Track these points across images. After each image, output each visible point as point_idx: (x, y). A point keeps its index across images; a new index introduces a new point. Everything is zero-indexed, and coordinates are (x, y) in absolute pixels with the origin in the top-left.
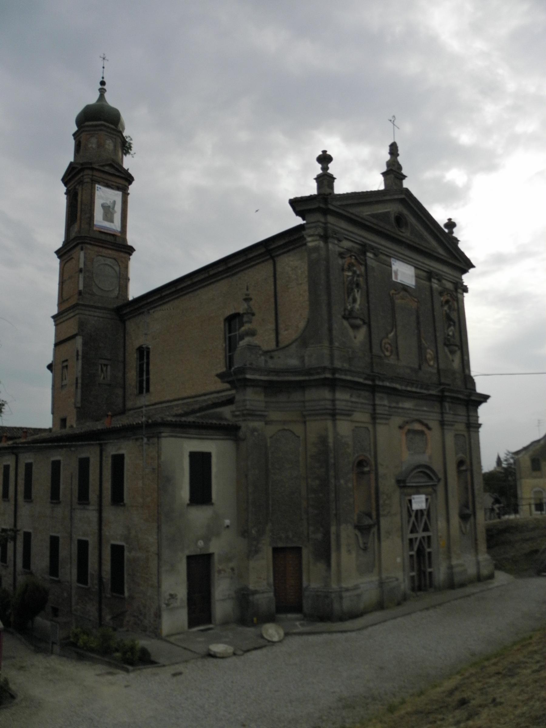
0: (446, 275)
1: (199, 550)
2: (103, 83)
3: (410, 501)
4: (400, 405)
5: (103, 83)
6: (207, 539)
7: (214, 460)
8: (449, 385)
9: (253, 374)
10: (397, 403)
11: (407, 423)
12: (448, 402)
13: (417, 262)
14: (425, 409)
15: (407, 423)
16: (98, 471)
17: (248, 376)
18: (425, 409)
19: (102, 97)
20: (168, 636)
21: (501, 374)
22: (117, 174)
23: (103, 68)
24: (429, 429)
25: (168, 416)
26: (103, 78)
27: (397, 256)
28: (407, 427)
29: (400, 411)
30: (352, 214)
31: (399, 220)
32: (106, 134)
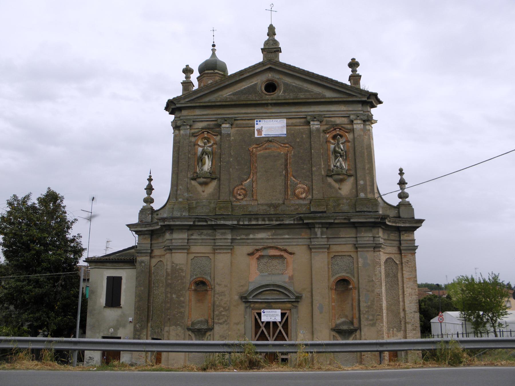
1: (110, 334)
2: (214, 46)
3: (259, 315)
4: (251, 236)
5: (214, 46)
6: (116, 328)
7: (124, 281)
8: (325, 212)
9: (136, 228)
10: (249, 235)
11: (257, 250)
12: (319, 227)
13: (287, 114)
14: (287, 236)
15: (257, 250)
18: (287, 236)
19: (214, 54)
21: (391, 193)
23: (214, 36)
26: (214, 42)
27: (260, 117)
30: (205, 102)
31: (271, 87)
32: (208, 78)
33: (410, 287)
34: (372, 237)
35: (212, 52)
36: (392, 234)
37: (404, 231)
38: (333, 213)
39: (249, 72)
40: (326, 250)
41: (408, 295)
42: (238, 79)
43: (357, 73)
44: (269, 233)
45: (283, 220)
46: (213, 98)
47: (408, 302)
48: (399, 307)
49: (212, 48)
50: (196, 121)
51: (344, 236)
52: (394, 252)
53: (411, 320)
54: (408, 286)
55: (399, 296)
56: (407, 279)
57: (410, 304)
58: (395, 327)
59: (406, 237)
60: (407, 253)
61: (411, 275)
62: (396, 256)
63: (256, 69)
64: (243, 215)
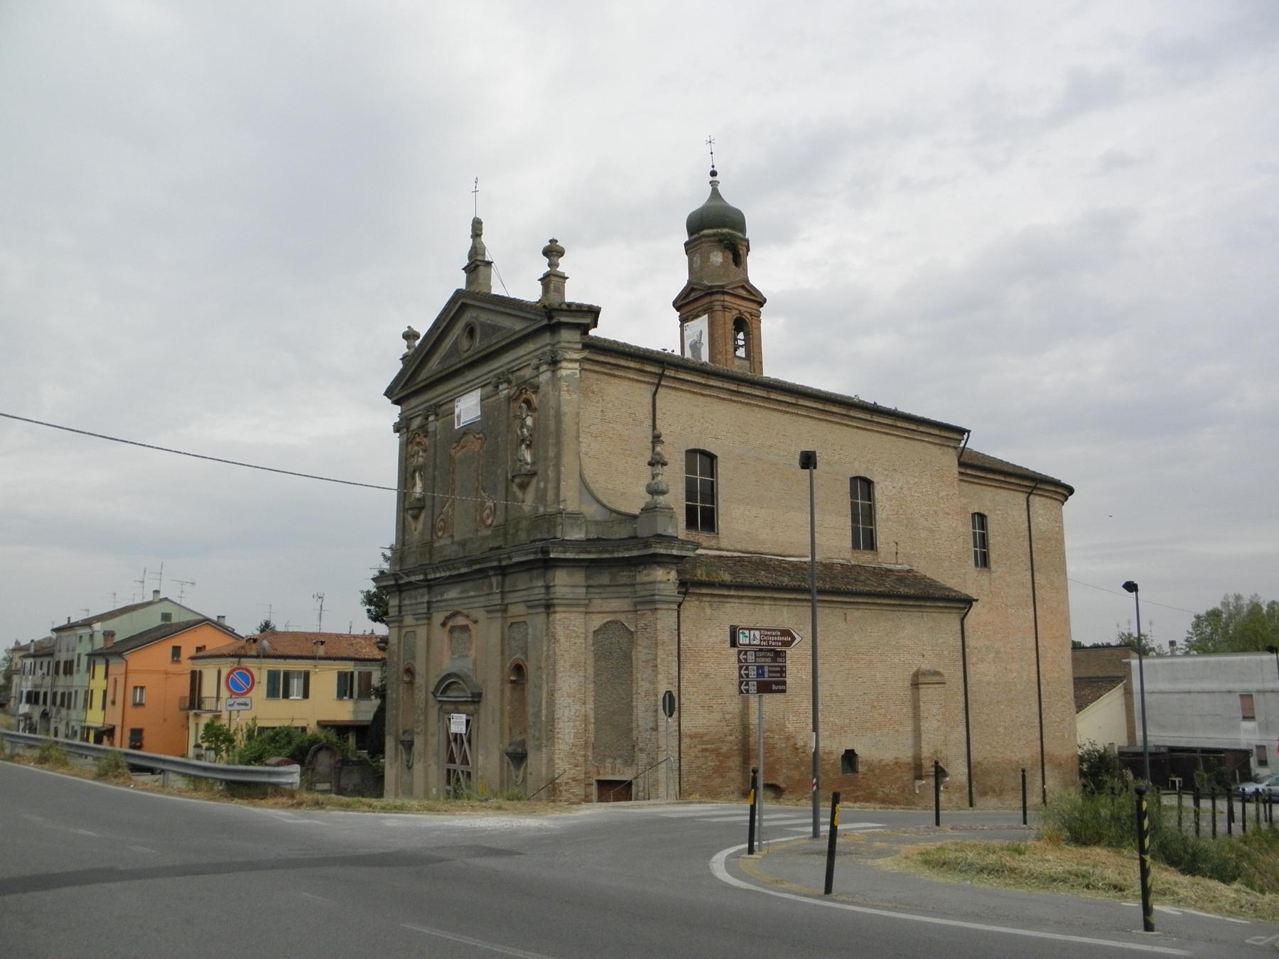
0: (513, 364)
2: (713, 174)
4: (445, 597)
5: (713, 174)
10: (442, 595)
14: (472, 593)
16: (122, 692)
17: (551, 556)
20: (215, 782)
22: (752, 298)
23: (712, 153)
24: (476, 622)
25: (746, 566)
26: (713, 167)
28: (450, 624)
29: (442, 604)
33: (646, 678)
34: (542, 586)
35: (710, 188)
36: (622, 574)
37: (642, 564)
38: (512, 547)
39: (444, 320)
40: (425, 622)
41: (643, 694)
42: (436, 336)
43: (558, 269)
44: (459, 590)
45: (613, 552)
46: (424, 374)
47: (644, 709)
48: (631, 718)
49: (711, 179)
50: (414, 417)
51: (523, 587)
52: (627, 609)
53: (647, 745)
54: (645, 676)
55: (632, 697)
56: (643, 662)
57: (646, 713)
58: (620, 757)
59: (646, 576)
60: (645, 610)
61: (648, 653)
62: (630, 616)
63: (450, 312)
64: (439, 562)
